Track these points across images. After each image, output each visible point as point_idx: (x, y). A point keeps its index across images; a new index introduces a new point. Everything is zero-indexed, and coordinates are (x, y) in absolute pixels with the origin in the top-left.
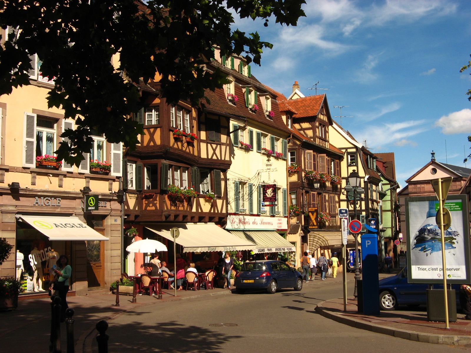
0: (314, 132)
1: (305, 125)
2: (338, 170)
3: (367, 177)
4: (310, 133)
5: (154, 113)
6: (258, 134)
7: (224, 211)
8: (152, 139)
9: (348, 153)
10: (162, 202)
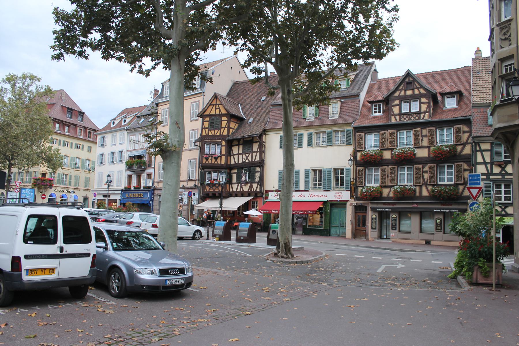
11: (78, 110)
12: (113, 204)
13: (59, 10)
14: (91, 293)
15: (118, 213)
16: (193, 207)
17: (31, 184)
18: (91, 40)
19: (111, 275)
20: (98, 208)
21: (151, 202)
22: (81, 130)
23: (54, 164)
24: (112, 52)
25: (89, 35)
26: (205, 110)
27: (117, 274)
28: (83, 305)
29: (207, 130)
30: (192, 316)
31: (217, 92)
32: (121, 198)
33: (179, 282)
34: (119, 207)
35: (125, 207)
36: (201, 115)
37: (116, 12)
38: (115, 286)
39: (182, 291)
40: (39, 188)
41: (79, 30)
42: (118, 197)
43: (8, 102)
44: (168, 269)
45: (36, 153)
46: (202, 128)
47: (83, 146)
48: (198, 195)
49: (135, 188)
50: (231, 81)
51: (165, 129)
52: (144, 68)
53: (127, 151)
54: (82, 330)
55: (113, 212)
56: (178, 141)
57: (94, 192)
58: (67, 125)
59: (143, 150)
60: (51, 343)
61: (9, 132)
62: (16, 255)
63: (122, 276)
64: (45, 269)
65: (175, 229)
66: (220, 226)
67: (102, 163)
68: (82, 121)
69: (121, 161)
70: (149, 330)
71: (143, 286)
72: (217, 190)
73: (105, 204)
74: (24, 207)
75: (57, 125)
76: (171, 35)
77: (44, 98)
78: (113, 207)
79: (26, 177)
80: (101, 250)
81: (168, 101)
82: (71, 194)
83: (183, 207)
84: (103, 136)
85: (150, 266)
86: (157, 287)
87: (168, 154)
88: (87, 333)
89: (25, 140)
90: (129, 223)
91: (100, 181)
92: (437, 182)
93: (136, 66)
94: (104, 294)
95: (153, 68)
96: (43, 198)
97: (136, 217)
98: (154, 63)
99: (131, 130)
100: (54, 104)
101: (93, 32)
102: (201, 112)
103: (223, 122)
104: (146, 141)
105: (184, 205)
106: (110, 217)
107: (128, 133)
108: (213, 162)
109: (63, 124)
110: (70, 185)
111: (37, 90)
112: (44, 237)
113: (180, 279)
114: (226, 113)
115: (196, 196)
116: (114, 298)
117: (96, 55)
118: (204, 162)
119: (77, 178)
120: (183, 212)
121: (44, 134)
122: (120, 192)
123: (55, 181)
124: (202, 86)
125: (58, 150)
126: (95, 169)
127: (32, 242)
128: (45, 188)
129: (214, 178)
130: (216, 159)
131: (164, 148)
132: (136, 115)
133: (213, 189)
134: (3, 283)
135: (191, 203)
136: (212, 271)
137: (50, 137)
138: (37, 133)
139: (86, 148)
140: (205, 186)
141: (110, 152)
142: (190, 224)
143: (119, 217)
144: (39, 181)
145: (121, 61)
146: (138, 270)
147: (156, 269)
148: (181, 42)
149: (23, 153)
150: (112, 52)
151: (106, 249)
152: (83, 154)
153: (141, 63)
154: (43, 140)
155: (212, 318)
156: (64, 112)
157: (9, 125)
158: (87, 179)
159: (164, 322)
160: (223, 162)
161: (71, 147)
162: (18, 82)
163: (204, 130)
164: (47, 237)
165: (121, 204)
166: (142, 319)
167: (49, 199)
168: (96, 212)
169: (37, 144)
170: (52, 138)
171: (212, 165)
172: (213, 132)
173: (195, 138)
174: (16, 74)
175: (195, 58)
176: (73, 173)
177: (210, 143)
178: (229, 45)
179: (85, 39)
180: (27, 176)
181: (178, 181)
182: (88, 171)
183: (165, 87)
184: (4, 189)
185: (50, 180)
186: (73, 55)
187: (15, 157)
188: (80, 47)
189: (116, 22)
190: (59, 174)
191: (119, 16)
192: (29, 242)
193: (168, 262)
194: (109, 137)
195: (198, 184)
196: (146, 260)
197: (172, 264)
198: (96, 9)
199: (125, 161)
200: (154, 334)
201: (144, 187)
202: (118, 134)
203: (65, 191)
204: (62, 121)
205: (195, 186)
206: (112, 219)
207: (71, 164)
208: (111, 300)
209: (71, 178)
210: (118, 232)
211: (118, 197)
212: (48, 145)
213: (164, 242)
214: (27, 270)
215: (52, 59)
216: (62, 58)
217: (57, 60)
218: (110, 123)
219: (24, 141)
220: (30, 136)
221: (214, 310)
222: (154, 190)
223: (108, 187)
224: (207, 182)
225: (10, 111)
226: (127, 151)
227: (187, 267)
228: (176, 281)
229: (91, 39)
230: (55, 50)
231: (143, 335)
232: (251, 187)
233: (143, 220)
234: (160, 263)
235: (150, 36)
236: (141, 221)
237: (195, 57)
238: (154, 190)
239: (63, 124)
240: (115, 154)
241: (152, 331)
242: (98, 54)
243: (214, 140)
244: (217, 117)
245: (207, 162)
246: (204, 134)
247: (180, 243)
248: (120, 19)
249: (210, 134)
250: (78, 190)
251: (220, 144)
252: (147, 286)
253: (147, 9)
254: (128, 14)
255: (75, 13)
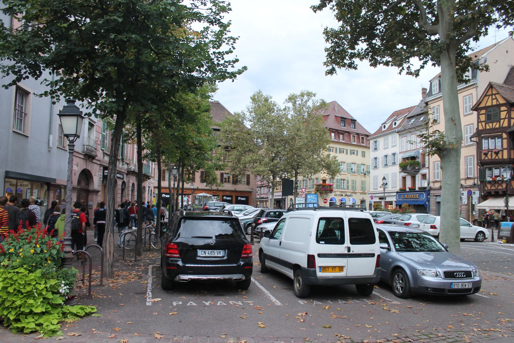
11: (350, 118)
12: (389, 206)
13: (328, 29)
14: (376, 292)
15: (394, 215)
16: (473, 206)
17: (314, 190)
18: (358, 51)
19: (394, 276)
20: (375, 210)
21: (427, 203)
22: (354, 136)
23: (333, 170)
24: (379, 59)
25: (356, 47)
26: (479, 103)
27: (401, 275)
28: (369, 302)
29: (484, 124)
30: (483, 324)
31: (492, 81)
32: (397, 199)
33: (465, 286)
34: (396, 209)
35: (400, 208)
36: (476, 108)
37: (379, 19)
38: (399, 286)
39: (468, 296)
40: (321, 193)
41: (347, 43)
42: (394, 199)
43: (291, 119)
44: (454, 272)
45: (317, 161)
46: (478, 122)
47: (357, 151)
48: (478, 194)
49: (410, 189)
50: (508, 66)
51: (441, 127)
52: (413, 69)
53: (400, 153)
54: (371, 327)
55: (390, 214)
56: (455, 138)
57: (370, 195)
58: (343, 134)
59: (415, 151)
60: (343, 334)
61: (294, 145)
62: (311, 254)
63: (406, 277)
64: (335, 267)
65: (457, 231)
66: (507, 227)
67: (376, 167)
68: (355, 128)
69: (394, 163)
70: (436, 333)
71: (427, 288)
72: (500, 188)
73: (381, 206)
74: (315, 210)
75: (333, 134)
76: (437, 30)
77: (320, 111)
78: (389, 208)
79: (309, 184)
80: (385, 251)
81: (441, 97)
82: (349, 197)
83: (462, 207)
84: (375, 140)
85: (434, 268)
86: (443, 290)
87: (445, 152)
88: (375, 330)
89: (307, 150)
90: (407, 225)
91: (376, 184)
93: (404, 68)
94: (388, 293)
95: (422, 67)
96: (325, 202)
97: (414, 218)
98: (422, 61)
99: (402, 132)
100: (328, 115)
101: (360, 42)
102: (475, 105)
103: (502, 113)
104: (422, 141)
105: (463, 205)
106: (388, 219)
107: (399, 135)
108: (493, 158)
109: (337, 132)
110: (348, 189)
111: (313, 104)
112: (331, 238)
113: (466, 283)
114: (505, 102)
115: (476, 195)
116: (398, 298)
117: (364, 64)
118: (483, 158)
119: (354, 182)
120: (462, 212)
121: (323, 144)
122: (395, 194)
123: (335, 186)
124: (474, 76)
125: (335, 158)
126: (369, 172)
127: (324, 242)
128: (326, 193)
129: (496, 175)
130: (497, 153)
131: (441, 146)
132: (406, 116)
133: (495, 186)
134: (302, 278)
135: (472, 202)
136: (502, 277)
137: (327, 146)
138: (316, 143)
139: (360, 153)
140: (486, 184)
141: (383, 156)
142: (471, 225)
143: (397, 218)
144: (321, 187)
145: (388, 65)
146: (422, 271)
147: (441, 271)
148: (449, 35)
149: (306, 162)
150: (379, 59)
151: (389, 249)
152: (358, 159)
153: (409, 64)
154: (322, 150)
155: (507, 329)
156: (338, 121)
157: (293, 138)
158: (363, 183)
159: (452, 327)
160: (505, 157)
161: (347, 153)
162: (298, 99)
163: (480, 124)
164: (334, 237)
165: (397, 205)
166: (428, 321)
167: (330, 203)
168: (374, 215)
169: (317, 153)
170: (329, 146)
171: (492, 161)
172: (491, 125)
173: (471, 133)
174: (296, 93)
175: (466, 49)
176: (350, 177)
177: (489, 137)
178: (504, 26)
179: (353, 51)
180: (310, 182)
181: (458, 179)
182: (363, 175)
183: (433, 85)
184: (292, 195)
185: (330, 186)
186: (344, 68)
187: (300, 167)
188: (349, 59)
189: (380, 29)
190: (337, 179)
191: (382, 22)
192: (321, 242)
193: (452, 265)
194: (381, 141)
195: (477, 182)
196: (428, 261)
197: (457, 267)
198: (360, 20)
199: (399, 163)
200: (442, 338)
201: (419, 188)
202: (390, 137)
203: (344, 195)
204: (337, 130)
205: (475, 184)
206: (390, 220)
207: (347, 169)
208: (397, 301)
209: (348, 183)
210: (399, 233)
211: (394, 199)
212: (326, 153)
213: (446, 243)
214: (320, 267)
215: (326, 75)
216: (334, 72)
217: (330, 75)
218: (381, 127)
219: (306, 152)
220: (311, 147)
221: (509, 320)
222: (429, 190)
223: (384, 189)
224: (489, 179)
225: (293, 126)
226: (400, 153)
227: (474, 271)
228: (462, 285)
229: (359, 49)
230: (328, 66)
231: (430, 338)
233: (421, 221)
234: (443, 265)
235: (414, 35)
236: (419, 223)
237: (465, 47)
238: (429, 190)
239: (337, 132)
240: (388, 157)
241: (440, 335)
242: (366, 62)
243: (493, 134)
244: (495, 108)
245: (486, 158)
246: (481, 128)
247: (463, 245)
248: (383, 25)
249: (488, 127)
250: (356, 193)
251: (500, 137)
252: (431, 288)
253: (409, 9)
254: (390, 18)
255: (342, 29)
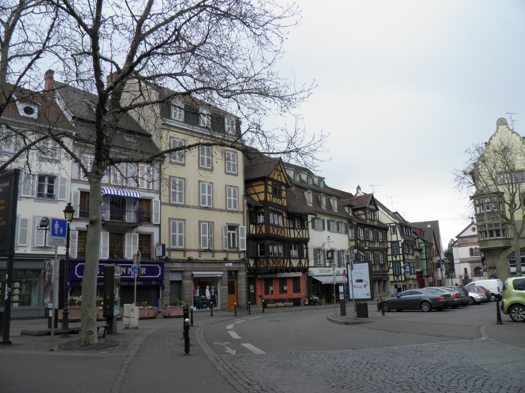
0: (366, 216)
1: (361, 212)
2: (204, 233)
3: (403, 240)
4: (363, 217)
5: (262, 217)
6: (328, 221)
7: (306, 266)
8: (261, 230)
9: (391, 227)
10: (268, 263)
72: (279, 265)
92: (45, 245)
232: (300, 262)
